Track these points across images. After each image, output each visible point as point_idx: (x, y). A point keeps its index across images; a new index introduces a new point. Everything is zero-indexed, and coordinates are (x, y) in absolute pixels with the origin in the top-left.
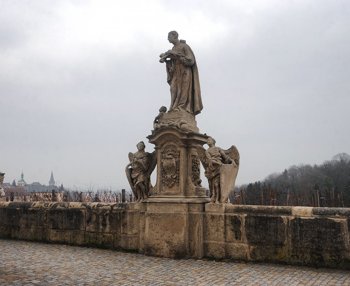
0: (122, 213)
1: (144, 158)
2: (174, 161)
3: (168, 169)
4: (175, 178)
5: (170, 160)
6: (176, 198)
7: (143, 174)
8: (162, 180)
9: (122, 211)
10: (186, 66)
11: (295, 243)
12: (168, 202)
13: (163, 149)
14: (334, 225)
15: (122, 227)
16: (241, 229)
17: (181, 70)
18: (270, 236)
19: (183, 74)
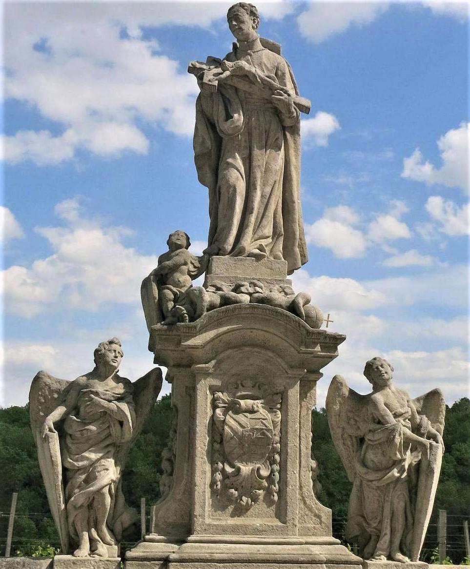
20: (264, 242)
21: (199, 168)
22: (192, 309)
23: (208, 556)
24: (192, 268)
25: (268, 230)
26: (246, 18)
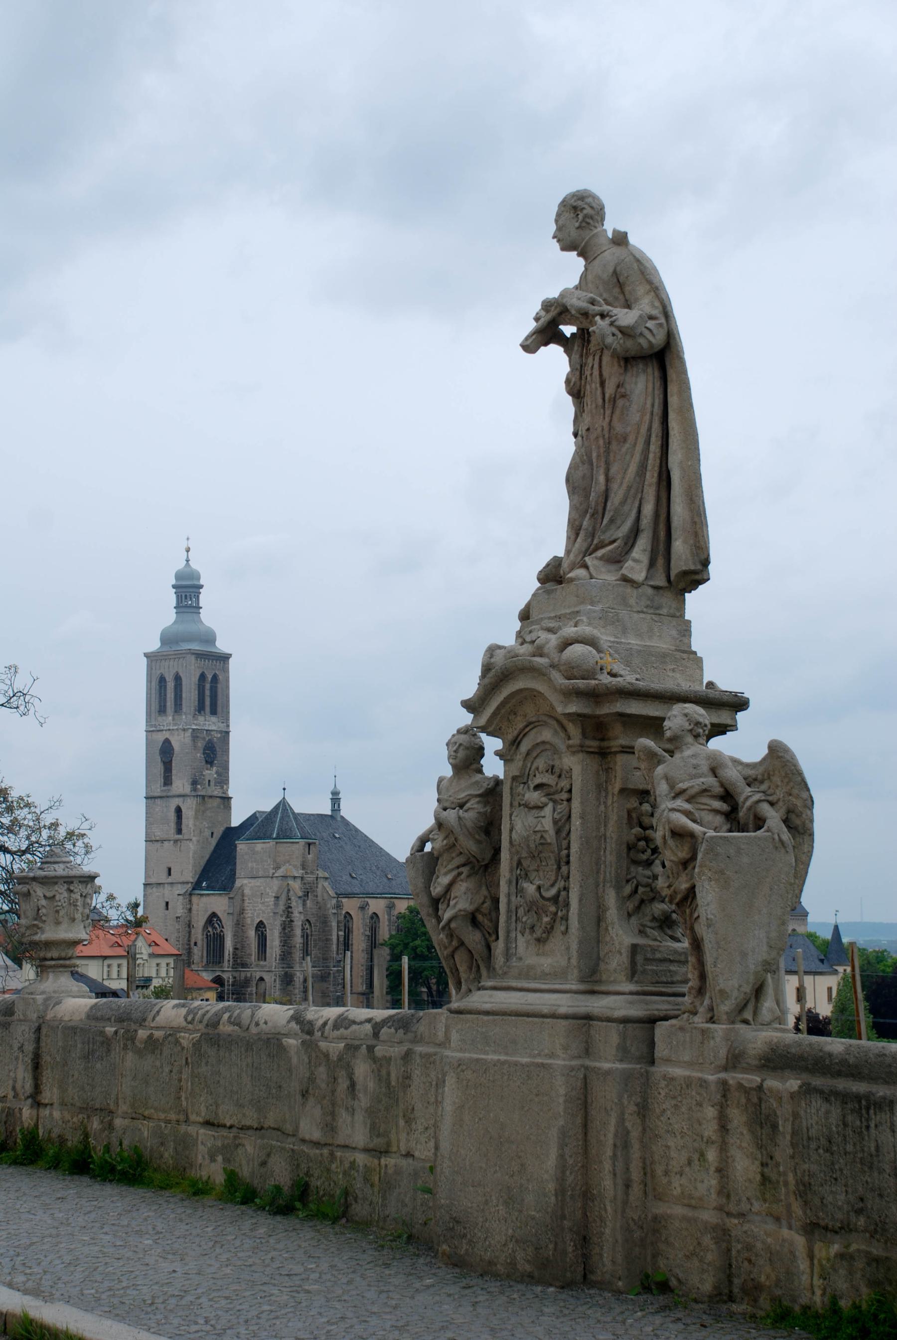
1: (468, 805)
4: (555, 899)
7: (469, 876)
10: (628, 361)
13: (521, 764)
17: (602, 384)
19: (614, 400)
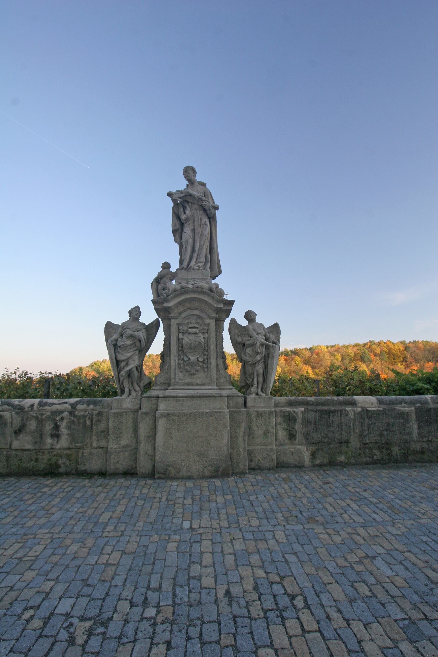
0: (96, 415)
2: (201, 337)
3: (191, 348)
5: (194, 335)
6: (184, 389)
8: (179, 364)
9: (95, 412)
11: (362, 438)
12: (197, 395)
14: (402, 415)
15: (94, 437)
16: (297, 427)
18: (333, 433)
20: (201, 265)
21: (174, 236)
22: (385, 391)
23: (175, 395)
24: (170, 276)
25: (203, 259)
26: (190, 172)
